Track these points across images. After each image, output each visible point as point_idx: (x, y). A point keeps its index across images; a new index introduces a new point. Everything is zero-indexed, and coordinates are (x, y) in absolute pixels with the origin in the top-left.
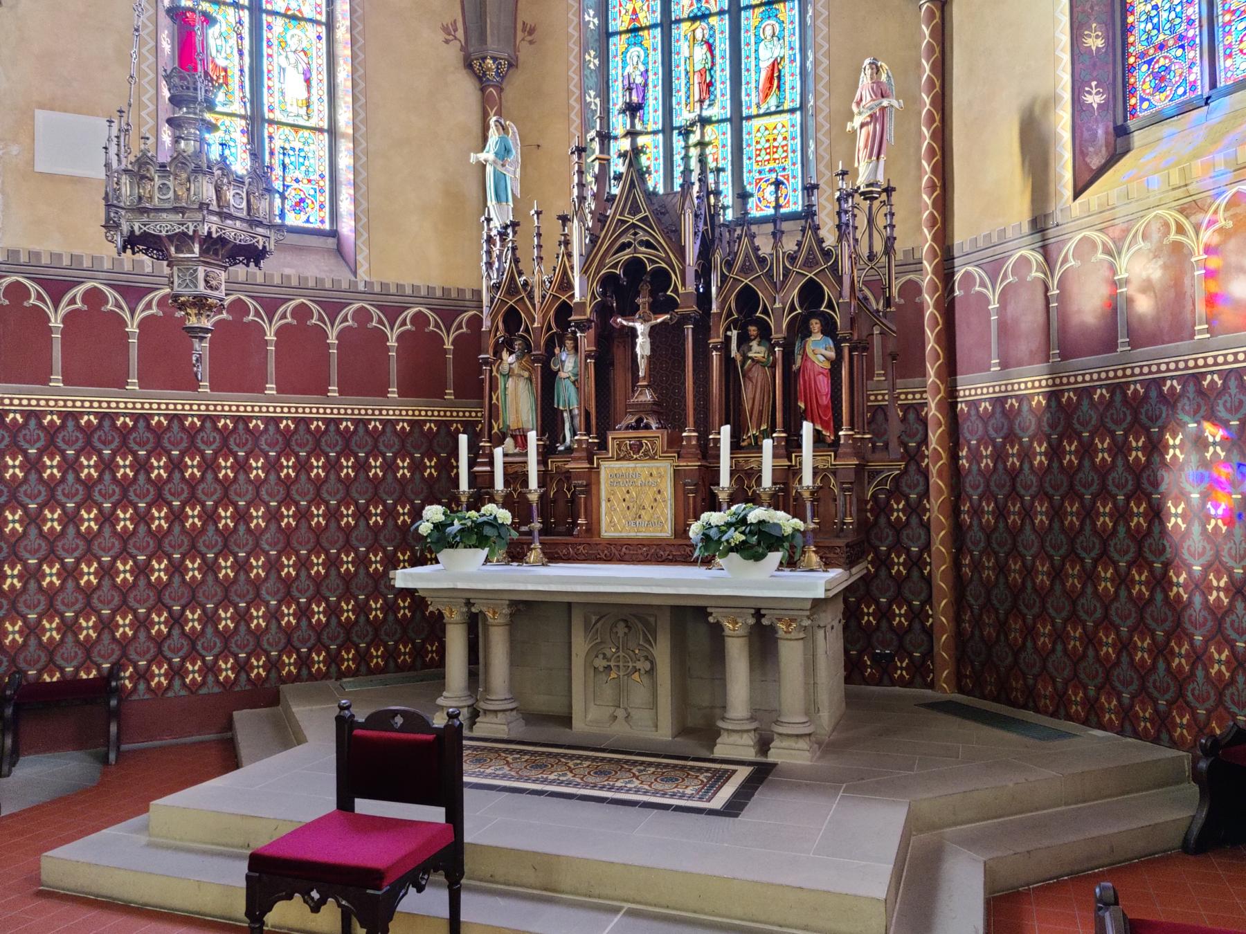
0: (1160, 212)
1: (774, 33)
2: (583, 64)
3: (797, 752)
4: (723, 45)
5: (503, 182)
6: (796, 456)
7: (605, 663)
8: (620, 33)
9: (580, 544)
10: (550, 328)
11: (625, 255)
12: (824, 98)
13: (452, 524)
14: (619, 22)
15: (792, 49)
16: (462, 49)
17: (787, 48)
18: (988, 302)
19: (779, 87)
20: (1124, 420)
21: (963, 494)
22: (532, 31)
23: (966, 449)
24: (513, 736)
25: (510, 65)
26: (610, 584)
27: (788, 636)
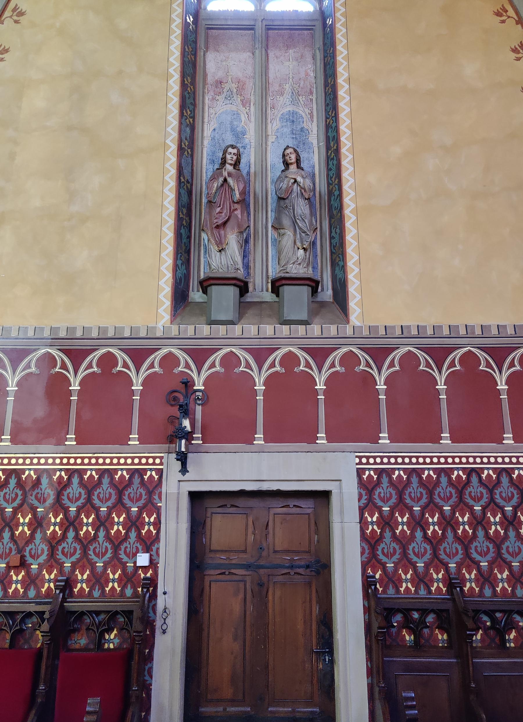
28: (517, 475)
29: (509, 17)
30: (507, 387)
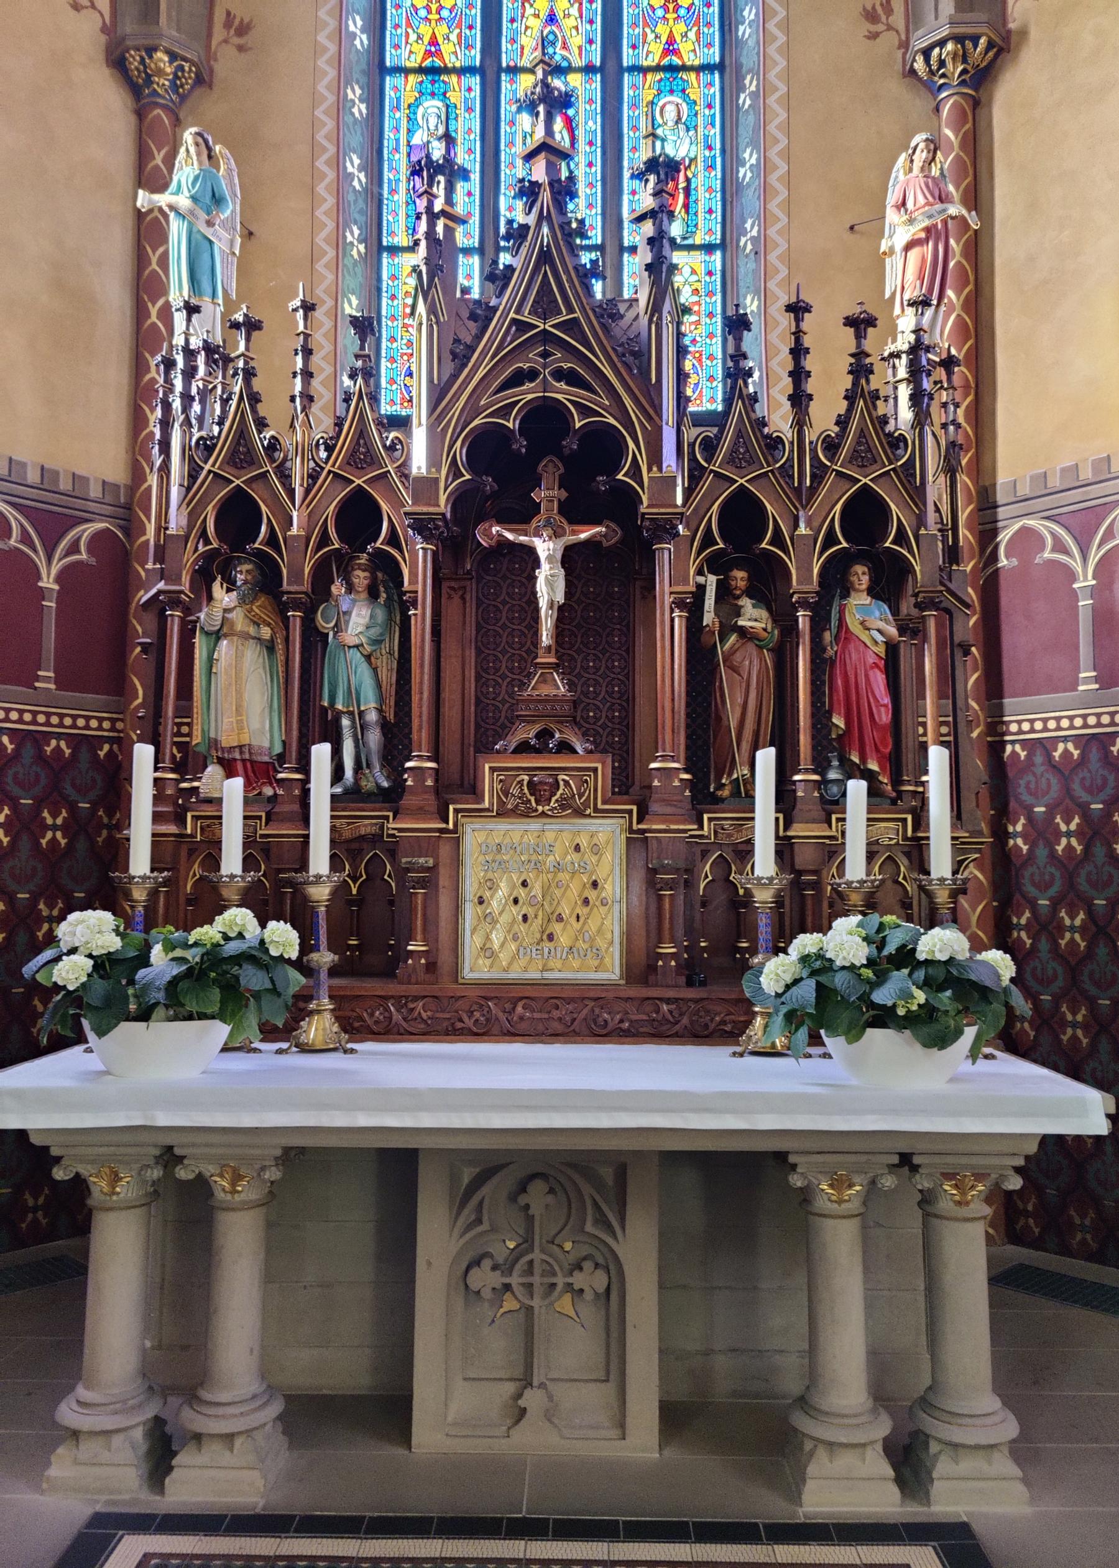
0: (1031, 522)
1: (679, 118)
2: (342, 106)
3: (991, 1484)
4: (590, 123)
5: (206, 257)
6: (838, 820)
7: (497, 1279)
8: (406, 71)
9: (416, 999)
10: (324, 540)
11: (528, 393)
12: (779, 226)
13: (144, 960)
14: (404, 52)
15: (710, 148)
16: (104, 29)
17: (701, 146)
18: (1072, 576)
19: (686, 206)
20: (1047, 793)
21: (1017, 896)
22: (243, 30)
23: (1022, 821)
24: (301, 1503)
25: (199, 81)
26: (575, 1109)
27: (964, 1212)
28: (53, 749)
29: (890, 28)
30: (56, 587)
